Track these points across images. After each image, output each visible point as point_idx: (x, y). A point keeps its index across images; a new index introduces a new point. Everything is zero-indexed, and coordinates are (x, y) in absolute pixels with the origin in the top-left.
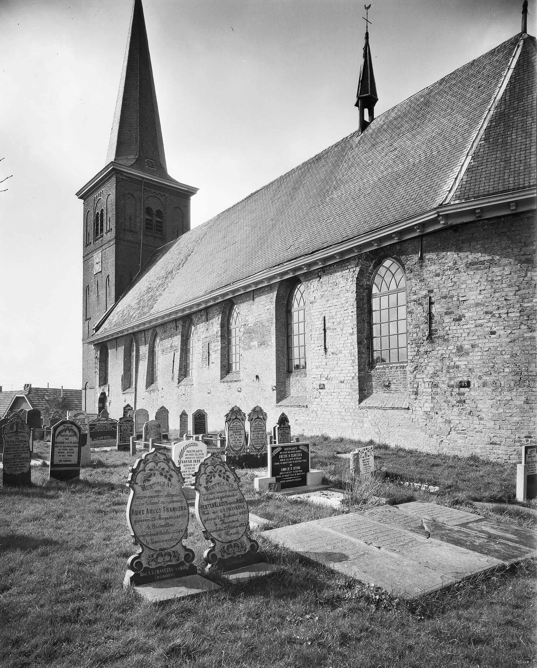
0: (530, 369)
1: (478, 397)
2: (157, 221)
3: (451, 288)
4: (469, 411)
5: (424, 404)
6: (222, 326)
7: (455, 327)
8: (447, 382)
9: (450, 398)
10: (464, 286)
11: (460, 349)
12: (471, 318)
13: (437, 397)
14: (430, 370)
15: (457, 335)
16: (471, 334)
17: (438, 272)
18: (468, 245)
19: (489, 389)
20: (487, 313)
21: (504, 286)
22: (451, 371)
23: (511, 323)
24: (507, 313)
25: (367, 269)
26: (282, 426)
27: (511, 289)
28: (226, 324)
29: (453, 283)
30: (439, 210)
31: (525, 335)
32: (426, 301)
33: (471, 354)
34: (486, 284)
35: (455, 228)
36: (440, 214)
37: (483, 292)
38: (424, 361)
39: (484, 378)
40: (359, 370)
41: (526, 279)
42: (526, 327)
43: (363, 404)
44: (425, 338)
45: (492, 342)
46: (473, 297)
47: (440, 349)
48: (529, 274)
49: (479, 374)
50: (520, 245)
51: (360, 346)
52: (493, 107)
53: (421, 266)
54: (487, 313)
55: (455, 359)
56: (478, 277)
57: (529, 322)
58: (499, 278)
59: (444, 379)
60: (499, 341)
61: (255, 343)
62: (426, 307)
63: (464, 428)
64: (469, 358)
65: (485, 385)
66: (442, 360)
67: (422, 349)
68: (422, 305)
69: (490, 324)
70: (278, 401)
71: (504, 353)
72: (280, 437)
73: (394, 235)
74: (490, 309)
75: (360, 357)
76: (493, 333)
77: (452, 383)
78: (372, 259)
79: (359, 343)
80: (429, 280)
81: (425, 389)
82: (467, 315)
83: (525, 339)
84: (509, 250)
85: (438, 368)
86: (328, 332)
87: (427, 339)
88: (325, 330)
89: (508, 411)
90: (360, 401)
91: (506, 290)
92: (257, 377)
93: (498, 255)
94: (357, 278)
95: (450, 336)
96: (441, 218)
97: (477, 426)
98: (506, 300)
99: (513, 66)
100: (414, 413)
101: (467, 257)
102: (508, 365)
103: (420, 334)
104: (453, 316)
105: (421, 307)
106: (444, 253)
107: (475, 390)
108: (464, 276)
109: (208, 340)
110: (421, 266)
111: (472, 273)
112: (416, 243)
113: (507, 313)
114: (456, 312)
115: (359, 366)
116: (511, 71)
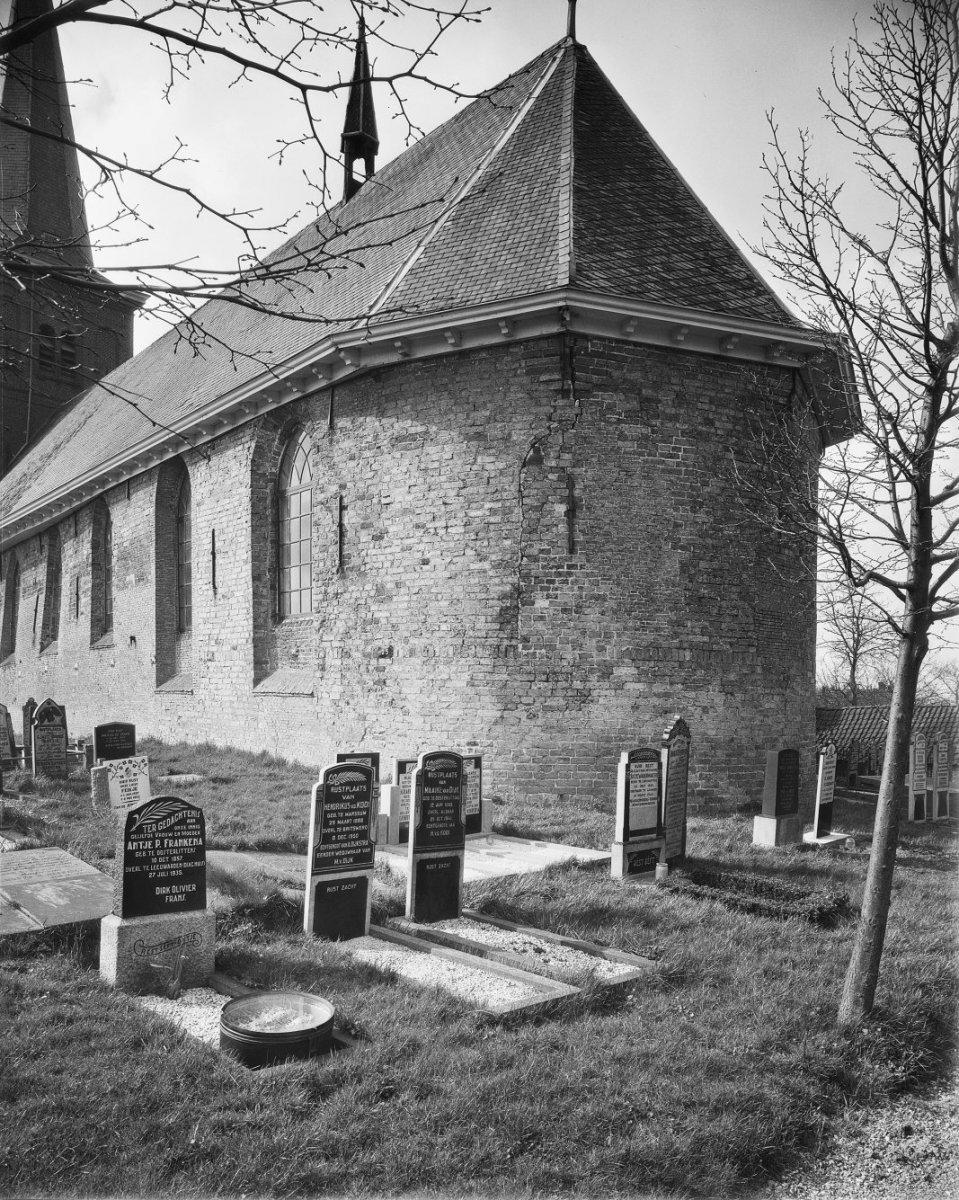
0: (478, 626)
1: (404, 676)
2: (63, 352)
3: (370, 482)
4: (390, 699)
5: (331, 689)
6: (95, 546)
7: (374, 552)
8: (362, 648)
9: (366, 677)
10: (387, 478)
11: (380, 589)
12: (396, 534)
13: (348, 674)
14: (340, 626)
15: (376, 565)
16: (396, 563)
17: (353, 452)
18: (393, 404)
19: (417, 661)
20: (417, 526)
21: (443, 478)
22: (368, 628)
23: (452, 544)
24: (447, 527)
25: (269, 446)
26: (46, 722)
27: (453, 485)
28: (102, 541)
29: (372, 473)
30: (336, 340)
31: (472, 566)
32: (335, 504)
33: (395, 599)
34: (417, 474)
35: (377, 373)
36: (341, 346)
37: (413, 489)
38: (332, 609)
39: (413, 641)
40: (255, 627)
41: (475, 467)
42: (473, 553)
43: (259, 688)
44: (334, 570)
45: (426, 578)
46: (400, 497)
47: (355, 590)
48: (479, 459)
49: (407, 634)
50: (466, 407)
51: (258, 583)
52: (486, 163)
53: (331, 441)
54: (417, 526)
55: (374, 608)
56: (406, 462)
57: (478, 543)
58: (436, 465)
59: (358, 642)
60: (433, 575)
61: (131, 578)
62: (336, 513)
63: (382, 730)
64: (393, 606)
65: (412, 653)
66: (357, 609)
67: (331, 590)
68: (331, 511)
69: (421, 547)
70: (160, 682)
71: (440, 596)
72: (40, 742)
73: (289, 384)
74: (422, 519)
75: (256, 604)
76: (426, 562)
77: (369, 649)
78: (275, 428)
79: (256, 578)
80: (341, 465)
81: (334, 661)
82: (391, 529)
83: (471, 573)
84: (451, 416)
85: (350, 624)
86: (218, 556)
87: (338, 571)
88: (213, 553)
89: (444, 699)
90: (257, 681)
91: (446, 486)
92: (133, 638)
93: (436, 424)
94: (253, 461)
95: (368, 566)
96: (342, 354)
97: (400, 726)
98: (445, 504)
99: (536, 94)
100: (321, 702)
101: (392, 426)
102: (444, 619)
103: (328, 563)
104: (372, 531)
105: (330, 515)
106: (362, 419)
107: (400, 663)
108: (387, 461)
109: (77, 570)
110: (331, 441)
111: (398, 455)
112: (326, 398)
113: (447, 527)
114: (376, 524)
115: (255, 620)
116: (532, 101)
